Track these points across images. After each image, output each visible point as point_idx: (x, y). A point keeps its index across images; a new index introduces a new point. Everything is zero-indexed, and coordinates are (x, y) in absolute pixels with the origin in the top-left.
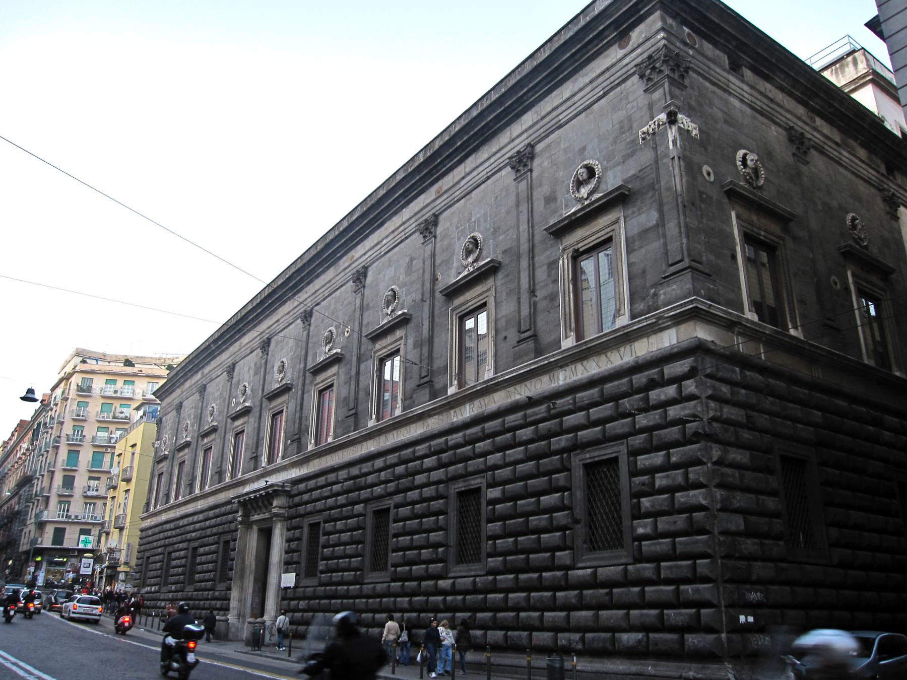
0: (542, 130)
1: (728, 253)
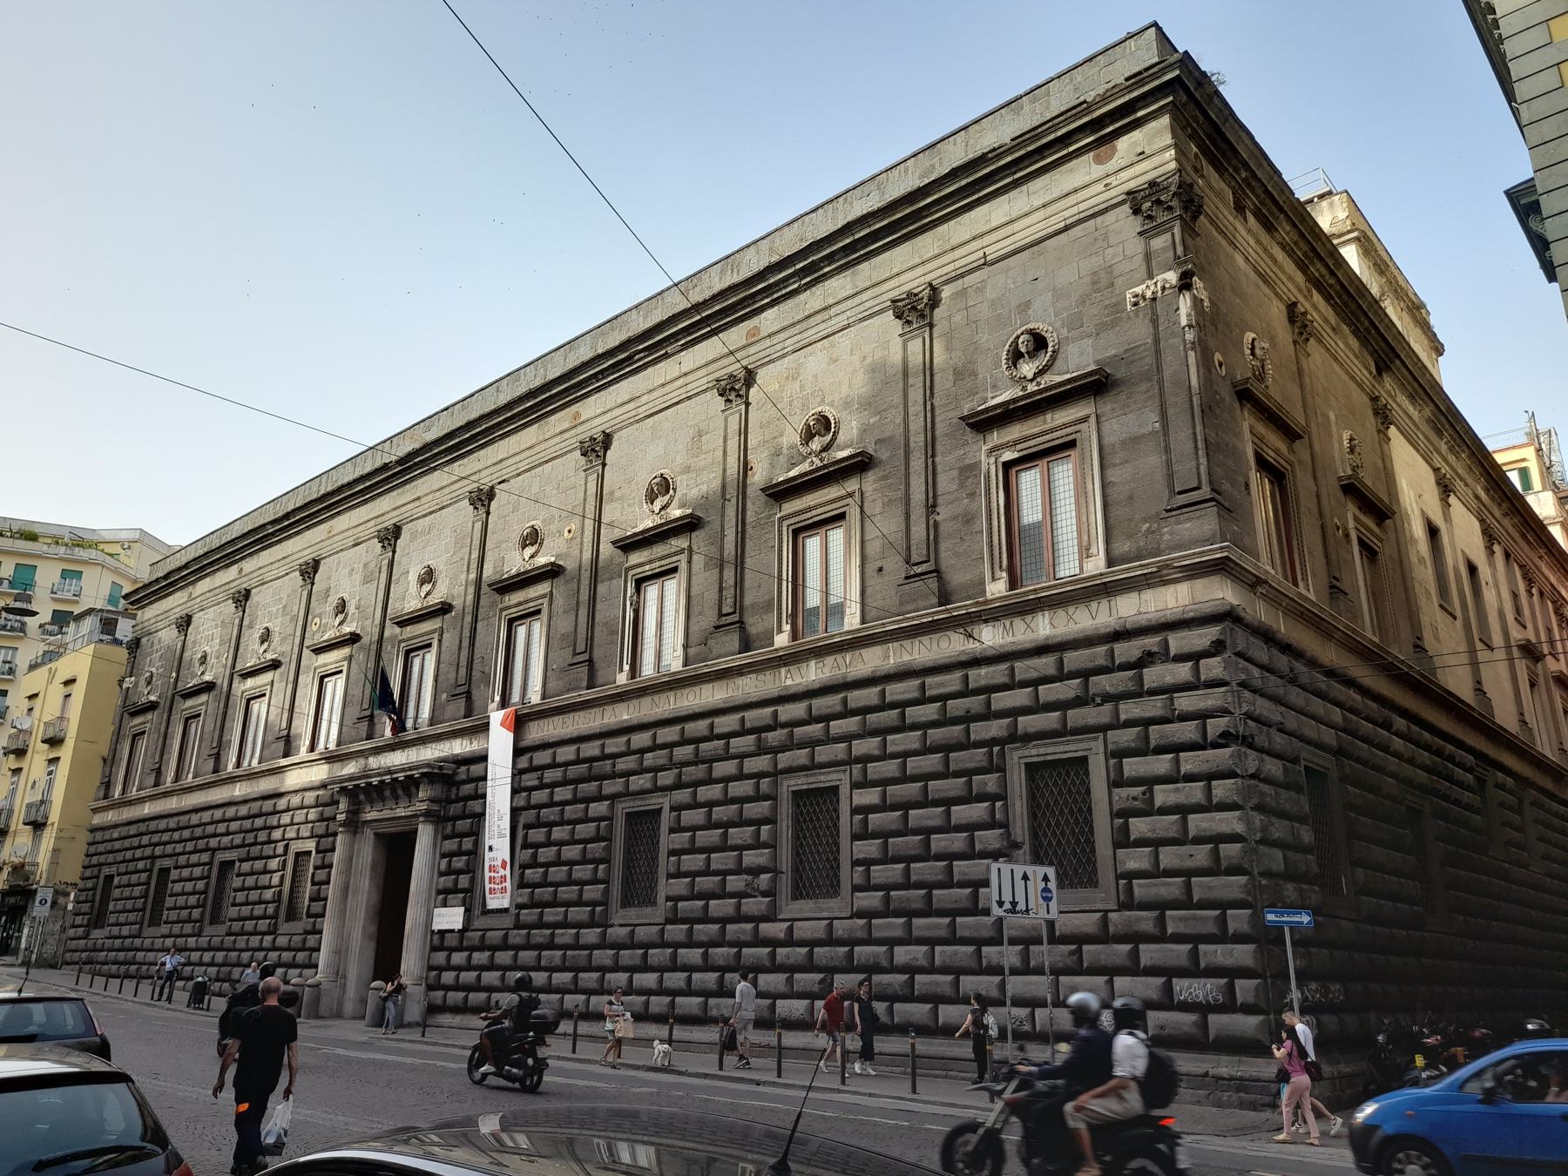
1: (1241, 479)
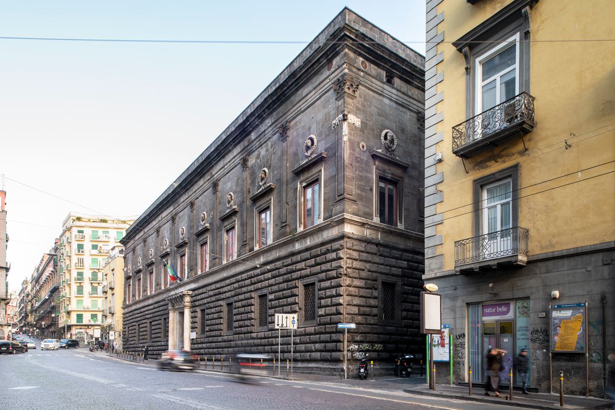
0: (293, 114)
